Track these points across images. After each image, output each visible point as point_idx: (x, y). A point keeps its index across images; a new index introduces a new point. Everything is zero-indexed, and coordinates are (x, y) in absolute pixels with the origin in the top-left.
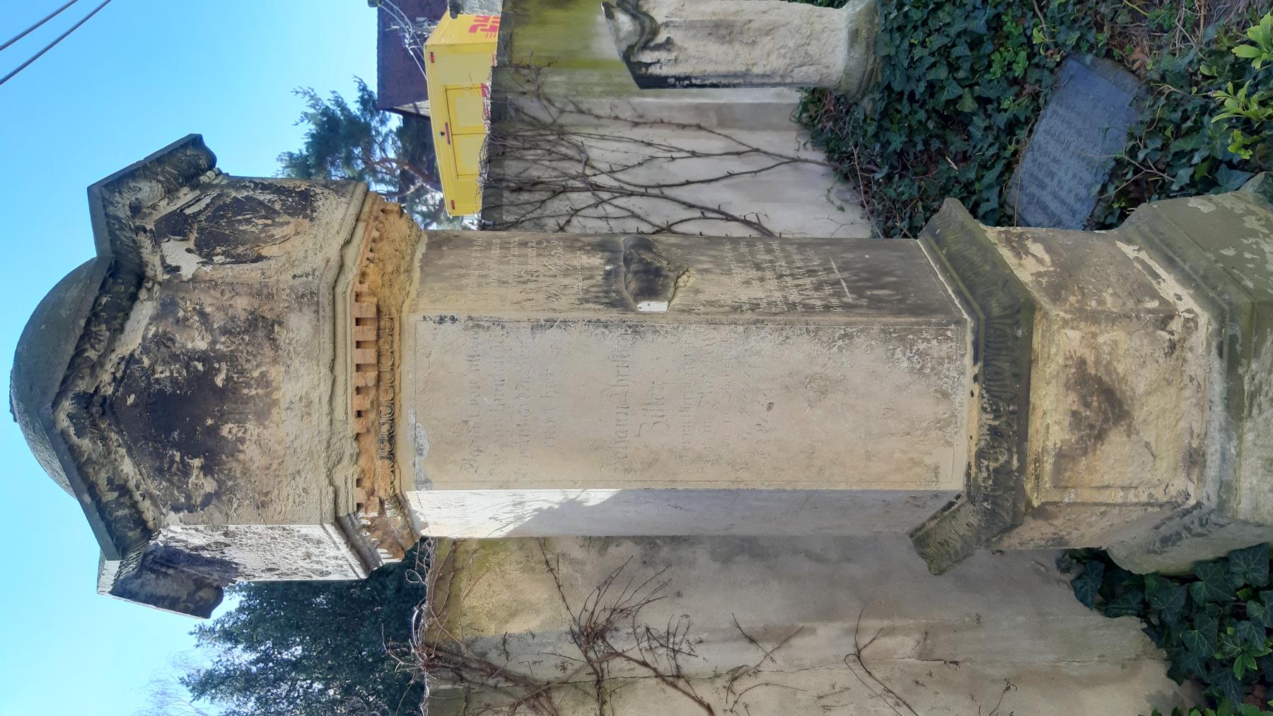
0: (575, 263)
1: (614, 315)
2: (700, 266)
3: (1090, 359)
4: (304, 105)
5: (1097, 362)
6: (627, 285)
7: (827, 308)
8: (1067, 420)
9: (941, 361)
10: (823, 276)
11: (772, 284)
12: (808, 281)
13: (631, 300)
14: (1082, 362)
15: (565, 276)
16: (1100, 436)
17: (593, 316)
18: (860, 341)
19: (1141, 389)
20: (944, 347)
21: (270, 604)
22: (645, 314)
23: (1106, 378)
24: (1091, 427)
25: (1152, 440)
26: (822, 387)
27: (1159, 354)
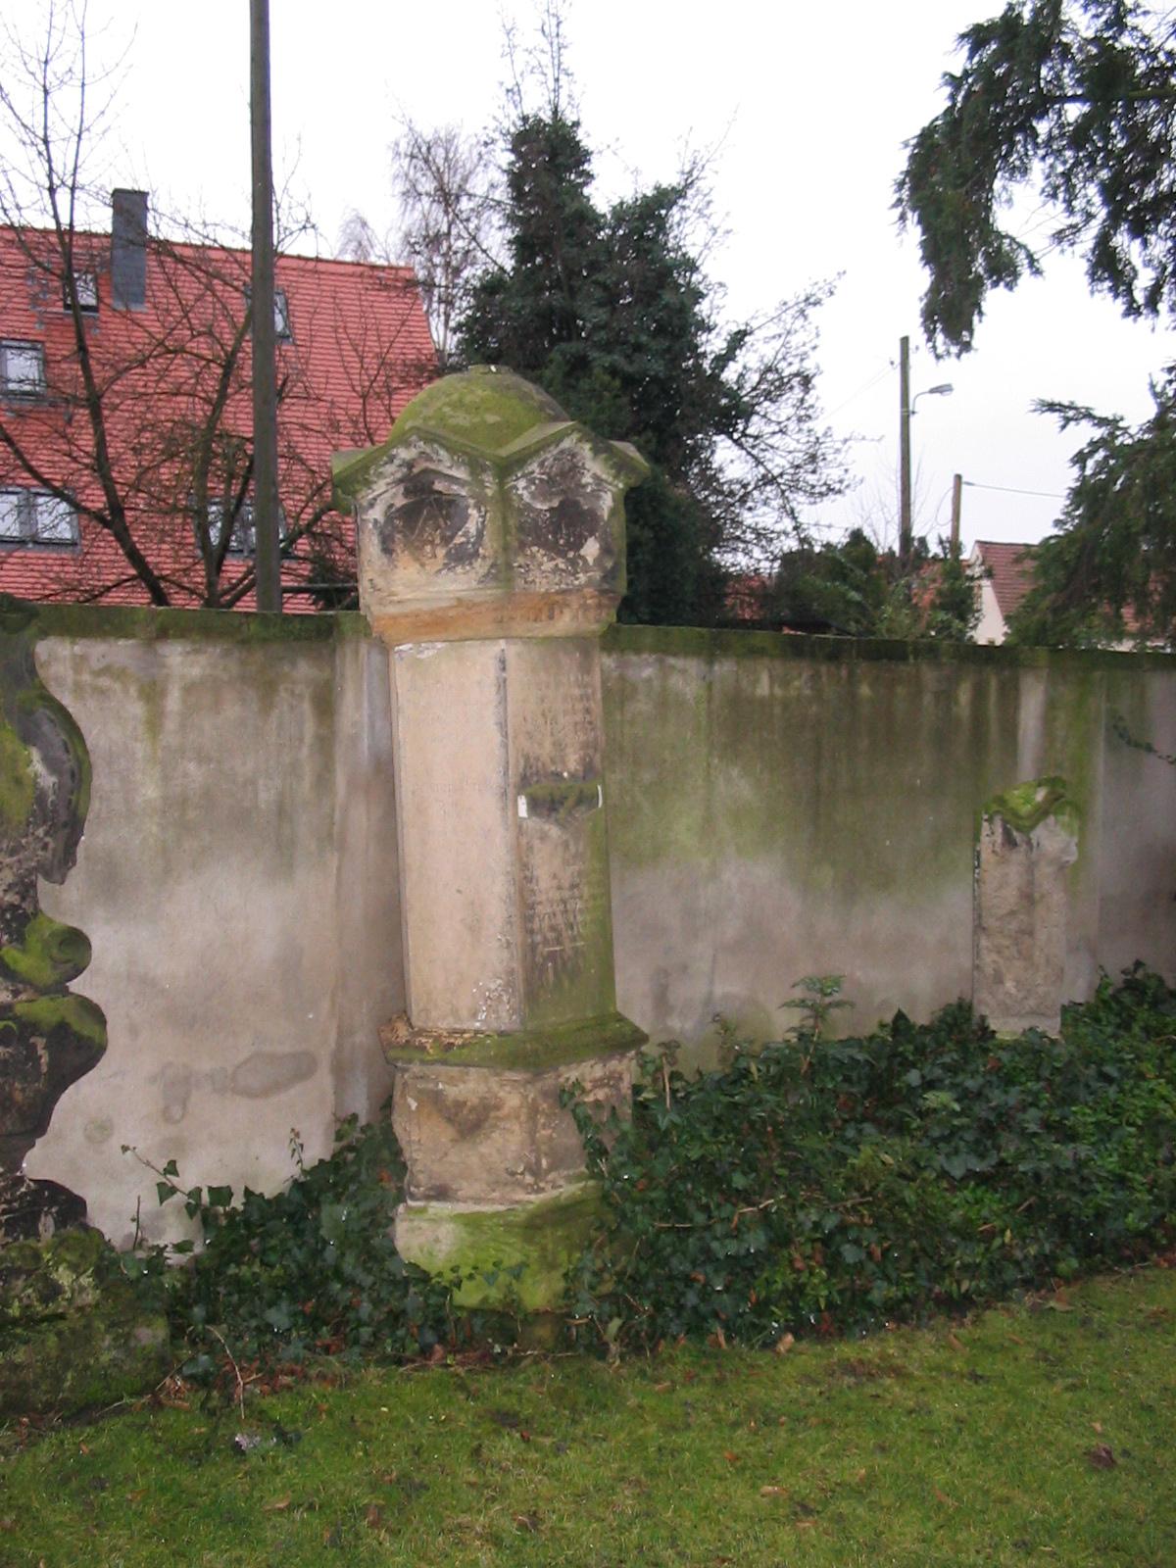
0: (569, 750)
1: (513, 779)
2: (571, 843)
3: (499, 1114)
4: (399, 132)
5: (498, 1118)
6: (542, 789)
7: (532, 932)
8: (461, 1099)
9: (496, 1012)
10: (567, 934)
11: (556, 895)
12: (560, 920)
13: (529, 790)
14: (498, 1108)
15: (554, 744)
16: (449, 1120)
17: (512, 761)
18: (505, 954)
19: (483, 1149)
20: (504, 1014)
21: (243, 1254)
22: (516, 801)
23: (487, 1125)
24: (456, 1114)
25: (449, 1158)
26: (474, 928)
27: (508, 1165)
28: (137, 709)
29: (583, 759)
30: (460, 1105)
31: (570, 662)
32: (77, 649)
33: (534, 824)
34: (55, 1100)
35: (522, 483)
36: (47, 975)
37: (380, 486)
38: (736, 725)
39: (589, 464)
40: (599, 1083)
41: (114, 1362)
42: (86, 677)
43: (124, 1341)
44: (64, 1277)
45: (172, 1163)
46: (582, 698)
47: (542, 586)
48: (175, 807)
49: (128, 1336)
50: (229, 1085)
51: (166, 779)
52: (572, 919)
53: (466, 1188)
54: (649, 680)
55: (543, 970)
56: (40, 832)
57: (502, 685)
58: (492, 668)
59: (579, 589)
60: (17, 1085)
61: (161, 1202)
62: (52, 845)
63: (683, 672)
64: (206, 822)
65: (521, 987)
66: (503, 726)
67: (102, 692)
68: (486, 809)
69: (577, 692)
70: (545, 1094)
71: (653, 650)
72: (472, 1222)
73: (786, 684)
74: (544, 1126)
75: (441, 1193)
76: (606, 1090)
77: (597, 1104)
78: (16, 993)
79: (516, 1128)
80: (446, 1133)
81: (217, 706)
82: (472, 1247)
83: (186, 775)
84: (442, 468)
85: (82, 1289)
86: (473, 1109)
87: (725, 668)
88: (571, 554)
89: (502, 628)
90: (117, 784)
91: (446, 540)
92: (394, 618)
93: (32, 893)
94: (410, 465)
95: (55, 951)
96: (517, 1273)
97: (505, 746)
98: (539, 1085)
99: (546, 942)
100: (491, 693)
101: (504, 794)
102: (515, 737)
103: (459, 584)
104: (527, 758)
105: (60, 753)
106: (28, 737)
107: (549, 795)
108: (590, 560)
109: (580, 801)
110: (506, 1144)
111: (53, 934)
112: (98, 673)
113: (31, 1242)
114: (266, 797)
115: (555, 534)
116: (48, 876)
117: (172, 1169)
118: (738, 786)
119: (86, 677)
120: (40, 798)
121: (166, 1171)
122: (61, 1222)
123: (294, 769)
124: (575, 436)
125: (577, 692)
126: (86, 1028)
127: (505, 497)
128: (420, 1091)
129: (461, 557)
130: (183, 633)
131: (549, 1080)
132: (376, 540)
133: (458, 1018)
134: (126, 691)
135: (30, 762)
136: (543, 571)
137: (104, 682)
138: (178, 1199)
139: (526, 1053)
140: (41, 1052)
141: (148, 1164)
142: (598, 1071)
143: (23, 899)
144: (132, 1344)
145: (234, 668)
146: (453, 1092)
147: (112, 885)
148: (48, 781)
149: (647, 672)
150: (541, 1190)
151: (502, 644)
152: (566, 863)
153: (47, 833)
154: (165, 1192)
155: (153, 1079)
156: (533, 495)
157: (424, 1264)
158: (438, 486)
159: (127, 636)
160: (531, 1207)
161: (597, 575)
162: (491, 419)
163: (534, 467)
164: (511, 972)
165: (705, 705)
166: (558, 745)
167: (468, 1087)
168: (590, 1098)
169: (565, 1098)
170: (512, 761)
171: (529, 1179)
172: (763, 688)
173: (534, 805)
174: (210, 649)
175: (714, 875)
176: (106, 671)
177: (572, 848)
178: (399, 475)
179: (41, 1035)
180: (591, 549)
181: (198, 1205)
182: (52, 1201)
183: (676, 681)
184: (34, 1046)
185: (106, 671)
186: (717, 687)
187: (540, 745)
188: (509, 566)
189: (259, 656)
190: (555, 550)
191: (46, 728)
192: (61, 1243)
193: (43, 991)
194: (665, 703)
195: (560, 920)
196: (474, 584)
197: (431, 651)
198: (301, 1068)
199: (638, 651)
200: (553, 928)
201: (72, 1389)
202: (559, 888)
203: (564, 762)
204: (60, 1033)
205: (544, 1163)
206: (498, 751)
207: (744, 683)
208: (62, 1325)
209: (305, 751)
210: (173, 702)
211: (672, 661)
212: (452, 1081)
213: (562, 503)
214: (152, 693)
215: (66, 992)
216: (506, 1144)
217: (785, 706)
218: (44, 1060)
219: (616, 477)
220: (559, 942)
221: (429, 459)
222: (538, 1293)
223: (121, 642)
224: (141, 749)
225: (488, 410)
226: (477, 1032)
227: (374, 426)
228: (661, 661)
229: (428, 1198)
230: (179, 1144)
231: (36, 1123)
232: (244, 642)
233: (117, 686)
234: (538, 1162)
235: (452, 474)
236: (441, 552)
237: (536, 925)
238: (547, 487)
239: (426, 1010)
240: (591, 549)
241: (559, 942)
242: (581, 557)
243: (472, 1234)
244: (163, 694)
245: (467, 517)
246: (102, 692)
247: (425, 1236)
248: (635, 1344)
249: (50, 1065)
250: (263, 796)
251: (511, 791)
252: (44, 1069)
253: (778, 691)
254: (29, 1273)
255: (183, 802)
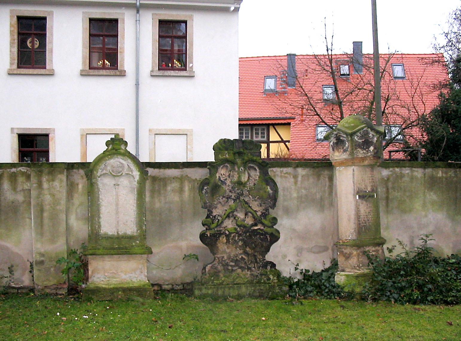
3: (353, 255)
7: (359, 221)
13: (359, 194)
14: (352, 254)
16: (344, 256)
17: (355, 189)
23: (350, 257)
26: (349, 220)
28: (292, 180)
29: (371, 189)
30: (346, 253)
31: (368, 170)
32: (281, 169)
33: (359, 201)
34: (271, 246)
35: (356, 137)
36: (270, 225)
37: (332, 138)
38: (432, 183)
39: (371, 132)
40: (373, 251)
41: (279, 292)
42: (283, 175)
43: (281, 289)
44: (271, 277)
45: (298, 264)
46: (371, 177)
47: (360, 156)
48: (300, 198)
49: (281, 288)
50: (310, 251)
51: (298, 192)
52: (369, 219)
53: (347, 270)
54: (408, 173)
55: (362, 228)
56: (269, 201)
57: (353, 175)
58: (352, 171)
59: (369, 156)
60: (264, 243)
61: (295, 270)
62: (271, 203)
63: (417, 171)
64: (306, 201)
65: (357, 231)
66: (354, 182)
67: (286, 177)
68: (351, 198)
69: (370, 176)
70: (361, 252)
71: (409, 167)
72: (347, 276)
73: (446, 173)
74: (361, 258)
75: (343, 271)
76: (375, 252)
77: (372, 255)
78: (264, 227)
79: (355, 258)
80: (344, 259)
81: (308, 180)
82: (347, 280)
83: (302, 192)
84: (342, 135)
85: (274, 279)
86: (348, 254)
87: (429, 171)
88: (367, 150)
89: (353, 164)
90: (288, 193)
91: (343, 148)
92: (335, 162)
93: (268, 211)
94: (336, 134)
95: (271, 221)
96: (354, 285)
97: (354, 186)
98: (360, 250)
99: (362, 223)
100: (352, 176)
101: (354, 195)
102: (356, 184)
103: (345, 156)
104: (359, 188)
105: (273, 187)
106: (267, 185)
107: (363, 196)
108: (371, 151)
109: (369, 197)
110: (354, 261)
111: (271, 218)
112: (285, 174)
113: (266, 270)
114: (318, 196)
115: (363, 146)
116: (271, 208)
117: (298, 265)
118: (432, 196)
119: (283, 175)
120: (269, 195)
121: (296, 265)
122: (271, 267)
123: (324, 191)
124: (366, 128)
125: (370, 176)
126: (277, 234)
127: (352, 140)
128: (340, 251)
129: (345, 151)
130: (301, 166)
131: (362, 249)
132: (331, 148)
133: (347, 238)
134: (290, 177)
135: (268, 188)
136: (361, 153)
137: (286, 175)
138: (299, 271)
139: (358, 245)
140: (268, 237)
141: (294, 264)
142: (374, 249)
143: (266, 211)
144: (282, 289)
145: (311, 172)
146: (345, 251)
147: (287, 211)
148: (271, 192)
149: (407, 172)
150: (360, 270)
151: (353, 167)
152: (367, 208)
153: (271, 201)
154: (296, 269)
155: (295, 248)
156: (358, 139)
157: (339, 283)
158: (341, 138)
159: (290, 167)
160: (358, 273)
161: (373, 153)
162: (352, 125)
163: (358, 134)
164: (355, 229)
165: (423, 179)
166: (366, 186)
167: (347, 251)
168: (371, 254)
169: (364, 253)
170: (355, 189)
171: (358, 268)
172: (440, 174)
173: (359, 196)
174: (307, 169)
175: (426, 216)
176: (287, 173)
177: (369, 205)
178: (335, 136)
179: (268, 234)
180: (372, 148)
181: (303, 272)
182: (270, 264)
183: (415, 174)
184: (267, 237)
185: (287, 173)
186: (426, 175)
187: (362, 185)
188: (353, 152)
189: (317, 170)
190: (364, 149)
191: (271, 183)
192: (271, 271)
193: (269, 227)
194: (412, 178)
195: (366, 219)
196: (347, 156)
197: (342, 168)
198: (326, 249)
199: (405, 167)
200: (364, 220)
201: (271, 295)
202: (366, 213)
203: (367, 189)
204: (272, 235)
205: (361, 265)
206: (353, 187)
207: (434, 173)
208: (270, 284)
209: (327, 188)
210: (300, 179)
211: (414, 169)
212: (345, 249)
213: (365, 140)
214: (295, 177)
215: (273, 228)
216: (354, 261)
217: (446, 179)
218: (269, 239)
219: (377, 134)
220: (365, 223)
221: (340, 133)
222: (358, 290)
223: (290, 168)
224: (293, 187)
225: (352, 123)
226: (350, 239)
227: (416, 105)
228: (411, 169)
229: (341, 271)
230: (300, 261)
231: (268, 250)
232: (314, 167)
233: (289, 176)
234: (360, 265)
235: (344, 137)
236: (342, 150)
237: (360, 220)
238: (361, 137)
239: (341, 236)
240: (372, 148)
241: (365, 223)
242: (369, 150)
243: (347, 278)
244: (298, 177)
245: (346, 144)
246: (286, 177)
247: (340, 278)
248: (374, 300)
249: (270, 240)
250: (318, 196)
251: (355, 194)
252: (269, 240)
253: (444, 175)
254: (265, 275)
255: (301, 197)
